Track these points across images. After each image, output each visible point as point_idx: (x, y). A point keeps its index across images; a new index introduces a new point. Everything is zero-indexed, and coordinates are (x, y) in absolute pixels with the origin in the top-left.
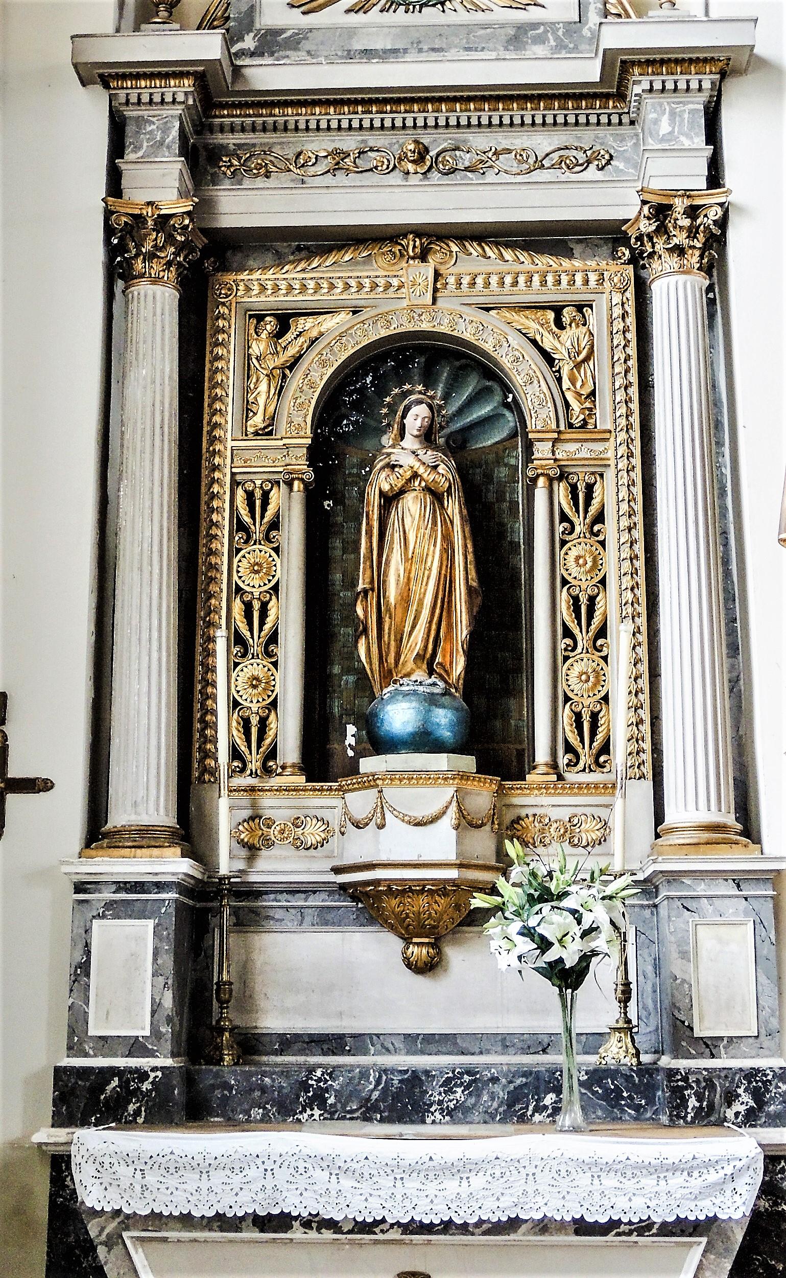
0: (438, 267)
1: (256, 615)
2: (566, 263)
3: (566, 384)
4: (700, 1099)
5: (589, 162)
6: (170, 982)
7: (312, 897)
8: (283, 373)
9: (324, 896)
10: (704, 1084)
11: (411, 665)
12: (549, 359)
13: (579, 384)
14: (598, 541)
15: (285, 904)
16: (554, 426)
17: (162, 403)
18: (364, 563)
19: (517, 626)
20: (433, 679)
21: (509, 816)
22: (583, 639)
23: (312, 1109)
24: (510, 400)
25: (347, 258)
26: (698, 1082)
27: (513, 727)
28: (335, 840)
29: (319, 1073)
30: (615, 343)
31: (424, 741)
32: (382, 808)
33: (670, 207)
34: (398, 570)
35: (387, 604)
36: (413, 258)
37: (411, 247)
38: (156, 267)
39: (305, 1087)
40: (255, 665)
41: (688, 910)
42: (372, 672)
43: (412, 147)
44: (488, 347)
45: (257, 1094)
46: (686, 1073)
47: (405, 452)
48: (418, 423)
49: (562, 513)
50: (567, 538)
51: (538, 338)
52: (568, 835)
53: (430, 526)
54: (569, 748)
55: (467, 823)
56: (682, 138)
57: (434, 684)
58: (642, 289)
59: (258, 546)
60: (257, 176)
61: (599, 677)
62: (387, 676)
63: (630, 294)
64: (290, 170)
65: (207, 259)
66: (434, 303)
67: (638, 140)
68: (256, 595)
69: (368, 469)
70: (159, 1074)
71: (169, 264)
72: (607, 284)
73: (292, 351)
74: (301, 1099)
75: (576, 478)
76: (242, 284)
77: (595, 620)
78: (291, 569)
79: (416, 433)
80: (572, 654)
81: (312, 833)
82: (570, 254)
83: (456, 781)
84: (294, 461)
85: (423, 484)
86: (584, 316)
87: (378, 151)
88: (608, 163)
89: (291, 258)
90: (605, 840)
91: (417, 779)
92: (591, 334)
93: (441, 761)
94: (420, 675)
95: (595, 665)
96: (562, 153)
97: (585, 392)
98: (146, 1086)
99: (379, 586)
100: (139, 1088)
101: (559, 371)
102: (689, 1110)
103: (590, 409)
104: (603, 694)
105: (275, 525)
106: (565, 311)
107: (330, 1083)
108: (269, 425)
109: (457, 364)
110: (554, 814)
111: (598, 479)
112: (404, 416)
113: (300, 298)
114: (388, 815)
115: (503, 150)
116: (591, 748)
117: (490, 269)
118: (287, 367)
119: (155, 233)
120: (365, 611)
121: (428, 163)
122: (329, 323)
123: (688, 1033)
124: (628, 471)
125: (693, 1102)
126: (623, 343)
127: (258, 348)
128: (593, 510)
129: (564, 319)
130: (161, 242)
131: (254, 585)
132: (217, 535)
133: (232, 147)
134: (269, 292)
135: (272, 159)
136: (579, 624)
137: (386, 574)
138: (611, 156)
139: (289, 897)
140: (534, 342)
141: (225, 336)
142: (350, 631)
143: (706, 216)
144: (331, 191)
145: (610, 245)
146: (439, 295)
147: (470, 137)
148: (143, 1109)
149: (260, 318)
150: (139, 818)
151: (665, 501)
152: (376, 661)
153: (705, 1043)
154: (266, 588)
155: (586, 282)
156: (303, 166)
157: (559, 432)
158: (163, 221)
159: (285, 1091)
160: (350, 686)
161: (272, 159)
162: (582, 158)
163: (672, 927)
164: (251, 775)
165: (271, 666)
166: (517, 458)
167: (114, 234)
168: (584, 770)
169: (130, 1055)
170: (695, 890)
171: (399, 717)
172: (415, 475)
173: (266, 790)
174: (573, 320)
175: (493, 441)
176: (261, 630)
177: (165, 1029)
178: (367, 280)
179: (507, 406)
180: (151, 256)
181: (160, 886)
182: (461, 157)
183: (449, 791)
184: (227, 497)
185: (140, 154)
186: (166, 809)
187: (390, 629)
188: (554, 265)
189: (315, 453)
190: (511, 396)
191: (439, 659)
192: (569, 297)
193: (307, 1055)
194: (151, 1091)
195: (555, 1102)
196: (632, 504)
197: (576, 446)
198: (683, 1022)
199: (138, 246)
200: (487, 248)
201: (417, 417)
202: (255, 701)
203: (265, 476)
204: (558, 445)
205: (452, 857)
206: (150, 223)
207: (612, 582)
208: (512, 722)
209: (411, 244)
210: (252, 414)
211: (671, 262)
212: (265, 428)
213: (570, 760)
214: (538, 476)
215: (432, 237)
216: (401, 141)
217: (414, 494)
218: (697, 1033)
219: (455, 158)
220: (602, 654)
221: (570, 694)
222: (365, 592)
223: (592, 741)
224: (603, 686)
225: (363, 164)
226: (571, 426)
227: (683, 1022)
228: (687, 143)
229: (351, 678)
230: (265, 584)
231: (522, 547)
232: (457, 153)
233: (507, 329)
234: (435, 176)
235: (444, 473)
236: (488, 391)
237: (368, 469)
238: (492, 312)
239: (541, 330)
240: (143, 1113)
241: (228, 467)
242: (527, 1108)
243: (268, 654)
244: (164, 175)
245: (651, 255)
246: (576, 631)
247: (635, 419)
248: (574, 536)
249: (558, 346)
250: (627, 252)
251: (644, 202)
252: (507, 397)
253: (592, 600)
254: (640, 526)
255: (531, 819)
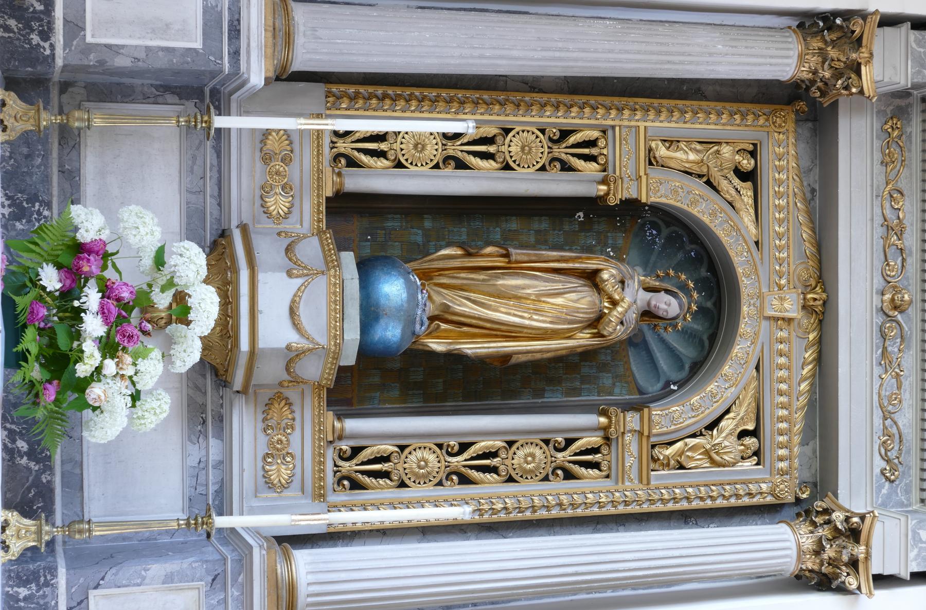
0: (796, 322)
1: (482, 148)
2: (797, 439)
3: (692, 442)
4: (26, 599)
5: (888, 461)
6: (140, 63)
7: (215, 202)
8: (704, 176)
9: (216, 213)
10: (42, 602)
11: (437, 299)
12: (712, 426)
13: (689, 454)
14: (547, 475)
15: (208, 175)
16: (654, 431)
17: (691, 63)
18: (535, 255)
19: (466, 398)
20: (427, 323)
21: (292, 394)
22: (457, 461)
23: (9, 206)
24: (672, 387)
25: (804, 236)
26: (44, 596)
27: (373, 394)
28: (269, 225)
29: (46, 213)
30: (727, 487)
31: (370, 314)
32: (307, 275)
33: (857, 541)
34: (529, 287)
35: (497, 277)
36: (805, 299)
37: (815, 296)
38: (814, 61)
39: (33, 199)
40: (436, 147)
41: (213, 580)
42: (430, 261)
43: (906, 297)
44: (726, 369)
45: (25, 150)
46: (52, 585)
47: (632, 292)
48: (663, 306)
49: (574, 440)
50: (551, 445)
51: (731, 415)
52: (275, 452)
53: (569, 317)
54: (356, 451)
55: (292, 357)
56: (916, 551)
57: (422, 325)
58: (768, 511)
59: (547, 150)
60: (883, 153)
61: (423, 479)
62: (426, 275)
63: (769, 499)
64: (887, 184)
65: (808, 107)
66: (769, 318)
67: (907, 506)
68: (503, 149)
69: (612, 254)
70: (48, 52)
71: (815, 72)
72: (778, 479)
73: (724, 185)
74: (20, 195)
75: (605, 452)
76: (785, 137)
77: (476, 473)
78: (525, 183)
79: (653, 303)
80: (444, 451)
81: (278, 203)
82: (803, 443)
83: (333, 348)
84: (625, 186)
85: (606, 311)
86: (749, 457)
87: (903, 266)
88: (887, 479)
89: (805, 184)
90: (269, 487)
91: (335, 309)
92: (734, 464)
93: (353, 335)
94: (431, 309)
95: (435, 474)
96: (897, 436)
97: (683, 460)
98: (35, 38)
99: (512, 268)
100: (32, 31)
101: (701, 435)
102: (15, 589)
103: (668, 465)
104: (407, 482)
105: (566, 167)
106: (754, 440)
107: (37, 224)
108: (657, 162)
109: (705, 337)
110: (295, 438)
111: (604, 473)
112: (667, 291)
113: (771, 193)
114: (299, 281)
115: (901, 382)
116: (356, 472)
117: (794, 369)
118: (709, 179)
119: (844, 60)
120: (489, 255)
121: (891, 313)
122: (748, 219)
123: (92, 584)
124: (612, 502)
125: (23, 592)
126: (727, 494)
127: (726, 150)
128: (576, 469)
129: (748, 439)
130: (837, 65)
131: (513, 147)
132: (558, 111)
133: (909, 130)
134: (777, 163)
135: (898, 167)
136: (472, 459)
137: (525, 276)
138: (893, 481)
139: (215, 180)
140: (728, 411)
141: (738, 122)
142: (464, 237)
143: (848, 574)
144: (869, 223)
145: (811, 480)
146: (772, 322)
147: (913, 352)
148: (11, 35)
149: (753, 154)
150: (301, 34)
151: (593, 542)
152: (441, 264)
153: (82, 601)
154: (508, 158)
155: (781, 459)
156: (891, 196)
157: (648, 437)
158: (856, 69)
159: (28, 179)
160: (413, 238)
161: (898, 167)
162: (892, 455)
163: (197, 564)
164: (332, 142)
165: (435, 162)
166: (620, 394)
167: (844, 20)
168: (336, 466)
169: (66, 22)
170: (232, 586)
171: (393, 289)
172: (614, 303)
173: (318, 158)
174: (747, 447)
175: (637, 375)
176: (469, 153)
177: (92, 59)
178: (786, 254)
179: (667, 384)
180: (822, 53)
181: (235, 54)
182: (895, 343)
183: (322, 340)
184: (593, 122)
185: (914, 46)
186: (310, 60)
187: (472, 279)
188: (796, 429)
189: (632, 206)
190: (676, 388)
191: (444, 326)
192: (768, 443)
193: (59, 197)
194: (30, 44)
195: (19, 451)
196: (583, 507)
197: (636, 454)
198: (103, 579)
199: (834, 43)
200: (810, 367)
201: (668, 305)
202: (403, 146)
203: (610, 158)
204: (636, 435)
205: (262, 344)
206: (854, 56)
207: (511, 488)
208: (378, 394)
209: (816, 295)
210: (668, 145)
211: (808, 542)
212: (655, 158)
213: (345, 452)
214: (609, 418)
215: (823, 316)
216: (910, 288)
217: (597, 302)
218: (92, 593)
219: (895, 337)
220: (444, 481)
221: (407, 451)
222: (507, 255)
223: (363, 473)
224: (414, 482)
225: (891, 252)
226: (653, 446)
227: (103, 579)
228: (912, 555)
229: (419, 239)
230: (511, 157)
231: (540, 401)
232: (899, 340)
233: (741, 386)
234: (879, 319)
235: (615, 330)
236: (681, 367)
237: (612, 254)
238: (754, 373)
239: (739, 418)
240: (6, 35)
241: (621, 123)
242: (13, 423)
243: (447, 159)
244: (894, 68)
245: (814, 524)
246: (466, 455)
247: (659, 507)
248: (553, 452)
249: (724, 435)
250: (804, 496)
251: (863, 518)
252: (674, 384)
253: (494, 470)
254: (562, 514)
255: (290, 416)
